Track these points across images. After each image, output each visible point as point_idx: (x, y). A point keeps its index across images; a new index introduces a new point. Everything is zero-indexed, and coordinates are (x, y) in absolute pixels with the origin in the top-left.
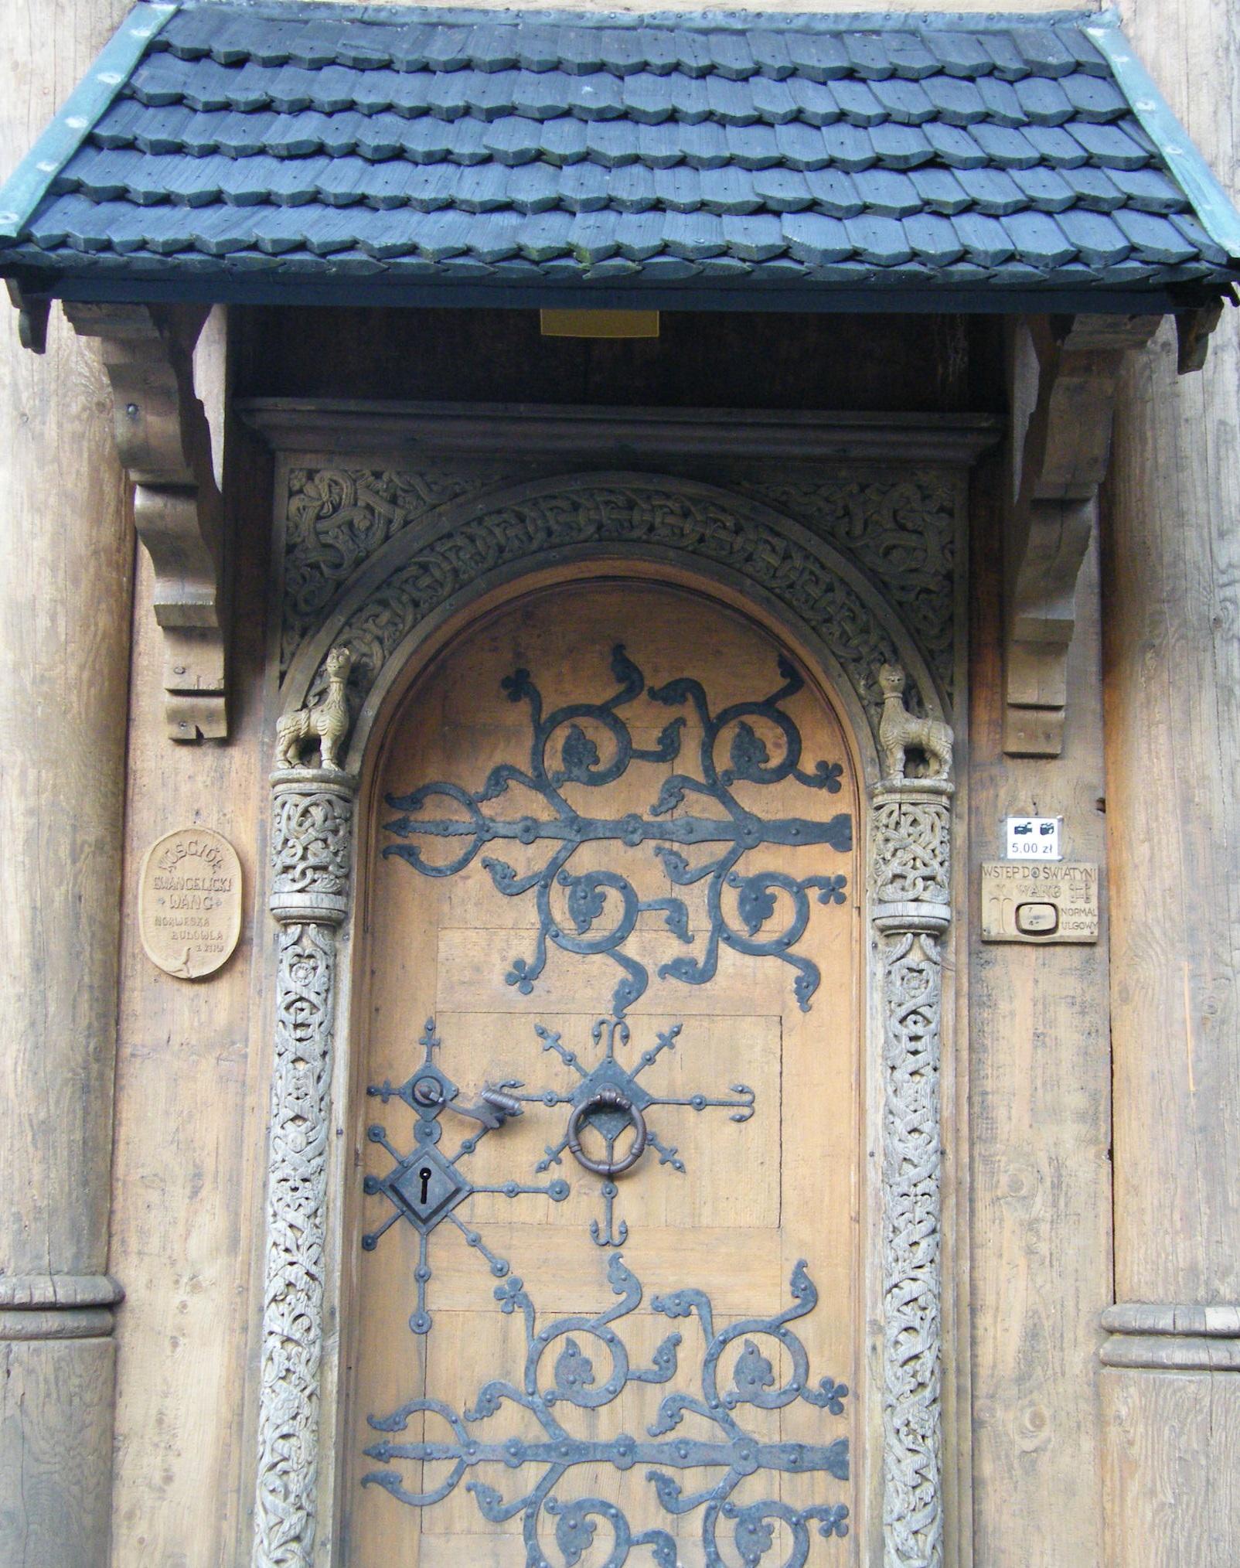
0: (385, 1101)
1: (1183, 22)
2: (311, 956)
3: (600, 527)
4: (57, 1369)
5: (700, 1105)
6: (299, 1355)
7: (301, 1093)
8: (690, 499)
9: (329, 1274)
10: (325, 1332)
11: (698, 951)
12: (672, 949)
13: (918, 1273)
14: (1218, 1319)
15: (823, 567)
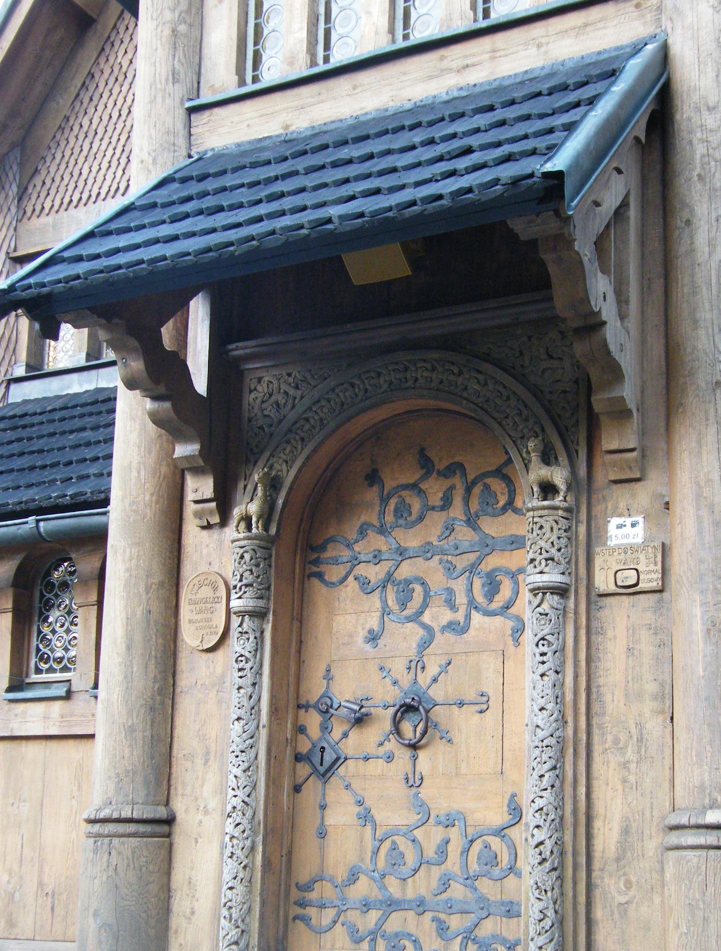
0: (307, 711)
1: (696, 28)
2: (246, 633)
3: (391, 383)
4: (133, 852)
5: (461, 704)
6: (238, 845)
7: (240, 705)
8: (436, 360)
9: (257, 801)
10: (254, 832)
11: (460, 616)
12: (447, 616)
13: (544, 794)
14: (712, 817)
15: (505, 387)
